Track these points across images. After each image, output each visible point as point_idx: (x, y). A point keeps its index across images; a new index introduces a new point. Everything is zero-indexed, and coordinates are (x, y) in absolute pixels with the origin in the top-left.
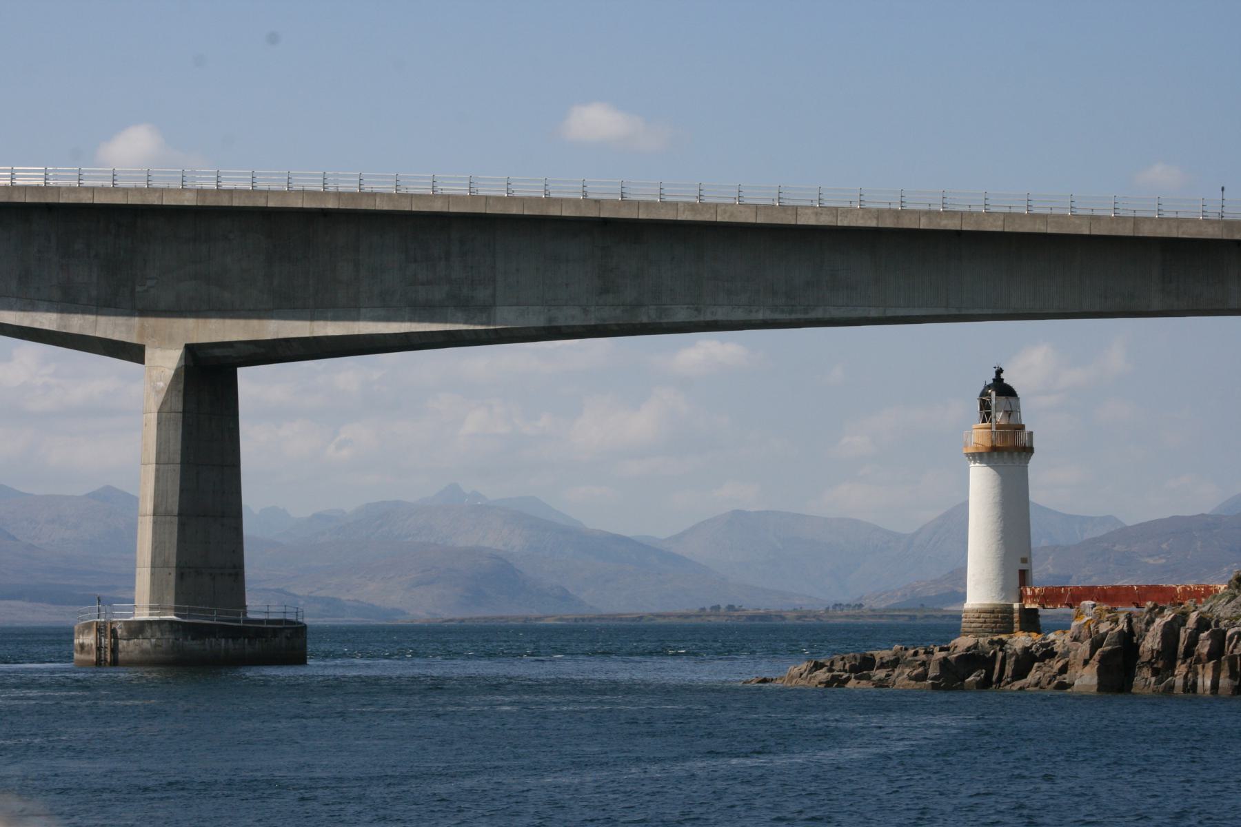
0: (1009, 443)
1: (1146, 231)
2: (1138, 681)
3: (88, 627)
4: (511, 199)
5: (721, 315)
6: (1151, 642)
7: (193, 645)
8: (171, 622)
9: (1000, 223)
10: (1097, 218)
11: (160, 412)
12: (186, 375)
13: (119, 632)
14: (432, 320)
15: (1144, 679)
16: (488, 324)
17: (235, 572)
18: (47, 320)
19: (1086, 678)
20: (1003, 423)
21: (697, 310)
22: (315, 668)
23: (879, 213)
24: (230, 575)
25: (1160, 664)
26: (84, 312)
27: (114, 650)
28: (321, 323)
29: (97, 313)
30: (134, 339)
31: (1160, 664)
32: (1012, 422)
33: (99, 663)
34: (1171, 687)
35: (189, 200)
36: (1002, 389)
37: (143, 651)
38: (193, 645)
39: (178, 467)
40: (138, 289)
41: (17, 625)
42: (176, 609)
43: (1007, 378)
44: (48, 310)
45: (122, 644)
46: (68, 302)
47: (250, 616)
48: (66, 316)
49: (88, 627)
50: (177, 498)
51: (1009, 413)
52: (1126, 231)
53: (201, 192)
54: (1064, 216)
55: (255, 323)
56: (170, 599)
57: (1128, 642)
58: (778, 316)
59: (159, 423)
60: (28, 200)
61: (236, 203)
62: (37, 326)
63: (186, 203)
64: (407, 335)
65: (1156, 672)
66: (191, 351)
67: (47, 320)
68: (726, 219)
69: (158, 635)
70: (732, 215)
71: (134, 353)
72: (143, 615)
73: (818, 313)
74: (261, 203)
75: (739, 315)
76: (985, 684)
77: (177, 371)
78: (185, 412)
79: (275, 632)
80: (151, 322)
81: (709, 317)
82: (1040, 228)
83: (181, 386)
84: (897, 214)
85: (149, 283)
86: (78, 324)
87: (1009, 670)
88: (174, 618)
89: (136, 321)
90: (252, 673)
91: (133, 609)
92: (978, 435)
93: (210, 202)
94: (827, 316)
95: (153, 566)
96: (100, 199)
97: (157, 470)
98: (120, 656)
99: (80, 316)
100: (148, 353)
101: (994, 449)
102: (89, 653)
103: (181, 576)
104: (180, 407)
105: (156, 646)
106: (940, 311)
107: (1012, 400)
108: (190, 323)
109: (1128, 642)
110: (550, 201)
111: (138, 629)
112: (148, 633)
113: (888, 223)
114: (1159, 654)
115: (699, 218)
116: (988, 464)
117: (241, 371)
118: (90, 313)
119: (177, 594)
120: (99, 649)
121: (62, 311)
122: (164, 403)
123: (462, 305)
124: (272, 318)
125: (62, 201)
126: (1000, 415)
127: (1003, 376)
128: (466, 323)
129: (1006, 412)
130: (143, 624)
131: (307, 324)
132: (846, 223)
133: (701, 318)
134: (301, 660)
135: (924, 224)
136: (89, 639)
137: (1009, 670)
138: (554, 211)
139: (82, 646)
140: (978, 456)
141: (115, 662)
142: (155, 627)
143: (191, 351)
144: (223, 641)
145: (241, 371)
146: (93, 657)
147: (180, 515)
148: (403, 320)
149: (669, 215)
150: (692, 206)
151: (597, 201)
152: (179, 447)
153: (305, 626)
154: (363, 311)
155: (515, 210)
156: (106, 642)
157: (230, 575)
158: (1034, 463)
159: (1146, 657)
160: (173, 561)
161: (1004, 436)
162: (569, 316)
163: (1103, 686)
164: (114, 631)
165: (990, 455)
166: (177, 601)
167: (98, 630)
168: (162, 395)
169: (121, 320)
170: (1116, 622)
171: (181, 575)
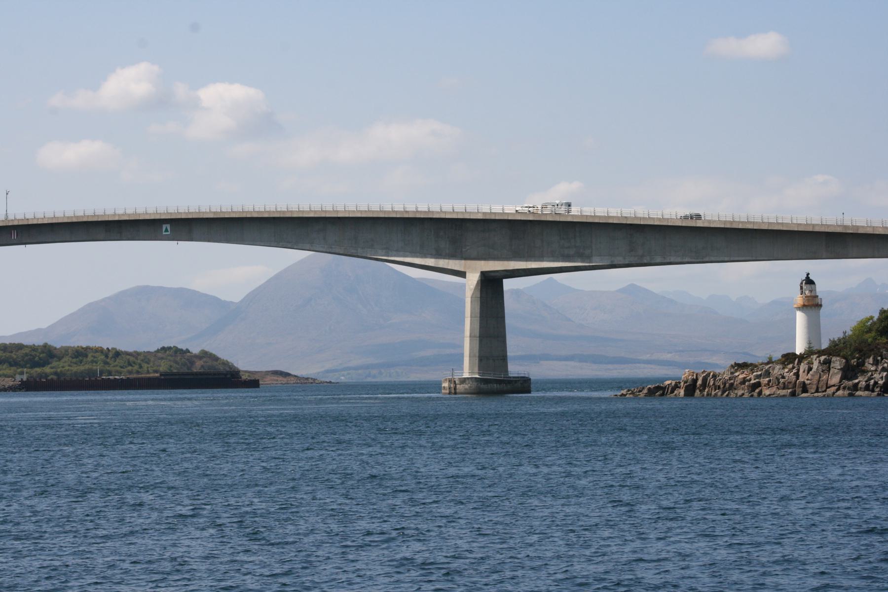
0: (811, 303)
1: (817, 229)
2: (696, 394)
3: (446, 380)
4: (595, 216)
5: (672, 260)
6: (699, 382)
7: (484, 386)
8: (476, 378)
9: (767, 226)
10: (800, 224)
11: (471, 298)
12: (481, 284)
13: (457, 382)
14: (569, 261)
15: (698, 392)
16: (590, 263)
17: (504, 358)
18: (430, 262)
19: (682, 392)
20: (809, 295)
21: (664, 258)
22: (534, 394)
23: (725, 222)
24: (501, 359)
25: (701, 388)
26: (444, 259)
27: (455, 389)
28: (530, 263)
29: (449, 259)
30: (462, 270)
31: (701, 388)
32: (813, 294)
33: (450, 393)
34: (703, 395)
35: (480, 217)
36: (809, 281)
37: (466, 389)
38: (484, 386)
39: (478, 319)
40: (464, 250)
41: (570, 377)
42: (479, 373)
43: (811, 277)
44: (431, 258)
45: (458, 386)
46: (438, 255)
47: (510, 375)
48: (437, 260)
49: (446, 380)
50: (478, 330)
51: (811, 291)
52: (810, 229)
53: (484, 213)
54: (789, 224)
55: (506, 263)
56: (476, 369)
57: (695, 381)
58: (693, 260)
59: (471, 302)
60: (422, 217)
61: (497, 218)
62: (427, 264)
63: (479, 218)
64: (561, 268)
65: (700, 391)
66: (483, 274)
67: (430, 262)
68: (671, 224)
69: (471, 383)
70: (249, 376)
71: (462, 274)
72: (466, 375)
73: (707, 259)
74: (506, 218)
75: (679, 260)
76: (662, 395)
77: (478, 282)
78: (481, 297)
79: (516, 381)
80: (469, 262)
81: (668, 261)
82: (781, 228)
83: (480, 288)
84: (731, 222)
85: (468, 248)
86: (443, 263)
87: (669, 391)
88: (478, 376)
89: (463, 262)
90: (511, 395)
91: (463, 373)
92: (799, 300)
93: (488, 217)
94: (710, 260)
95: (470, 357)
96: (448, 216)
97: (471, 320)
98: (457, 391)
99: (442, 260)
100: (467, 275)
101: (804, 306)
102: (446, 390)
103: (480, 360)
104: (479, 296)
105: (470, 387)
106: (751, 258)
107: (813, 286)
108: (483, 262)
109: (695, 381)
110: (609, 217)
111: (464, 381)
112: (467, 382)
113: (728, 226)
114: (701, 385)
115: (662, 224)
116: (802, 311)
117: (504, 280)
118: (446, 259)
119: (479, 366)
120: (450, 388)
121: (436, 258)
122: (473, 294)
123: (581, 256)
124: (512, 261)
125: (434, 217)
126: (807, 292)
127: (809, 276)
128: (582, 262)
129: (810, 290)
130: (465, 379)
131: (525, 263)
132: (713, 226)
133: (665, 261)
134: (529, 392)
135: (740, 226)
136: (446, 385)
137: (669, 391)
138: (611, 221)
139: (444, 387)
140: (799, 309)
141: (455, 393)
142: (470, 380)
143: (483, 274)
144: (495, 385)
145: (504, 280)
146: (448, 391)
147: (479, 337)
148: (559, 261)
149: (651, 223)
150: (659, 219)
151: (626, 217)
152: (479, 311)
153: (530, 379)
154: (545, 258)
155: (596, 221)
156: (452, 386)
157: (501, 359)
158: (822, 310)
159: (698, 386)
160: (477, 355)
161: (808, 300)
162: (619, 260)
163: (685, 395)
164: (455, 382)
165: (804, 308)
166: (479, 370)
167: (449, 381)
168: (473, 291)
169: (457, 262)
170: (693, 376)
171: (481, 360)
